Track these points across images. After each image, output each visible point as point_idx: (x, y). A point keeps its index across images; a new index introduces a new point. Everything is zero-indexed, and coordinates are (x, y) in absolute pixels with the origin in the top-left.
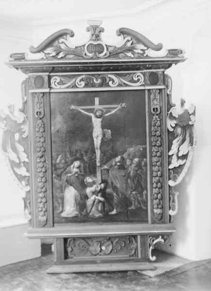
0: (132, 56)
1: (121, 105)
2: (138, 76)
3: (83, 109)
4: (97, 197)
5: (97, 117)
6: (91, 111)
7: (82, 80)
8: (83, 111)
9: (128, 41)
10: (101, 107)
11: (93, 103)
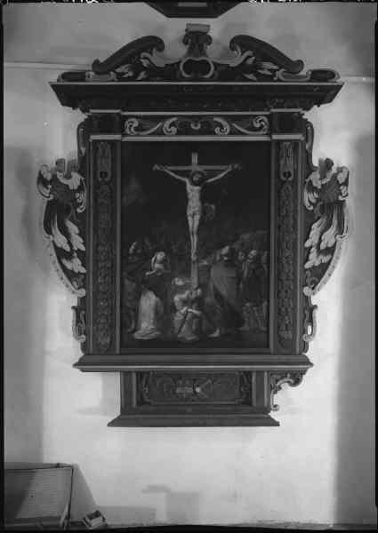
0: (255, 78)
1: (233, 167)
2: (260, 121)
3: (173, 171)
4: (190, 310)
5: (194, 184)
6: (186, 174)
7: (172, 125)
8: (172, 174)
9: (249, 57)
10: (200, 169)
11: (189, 162)
